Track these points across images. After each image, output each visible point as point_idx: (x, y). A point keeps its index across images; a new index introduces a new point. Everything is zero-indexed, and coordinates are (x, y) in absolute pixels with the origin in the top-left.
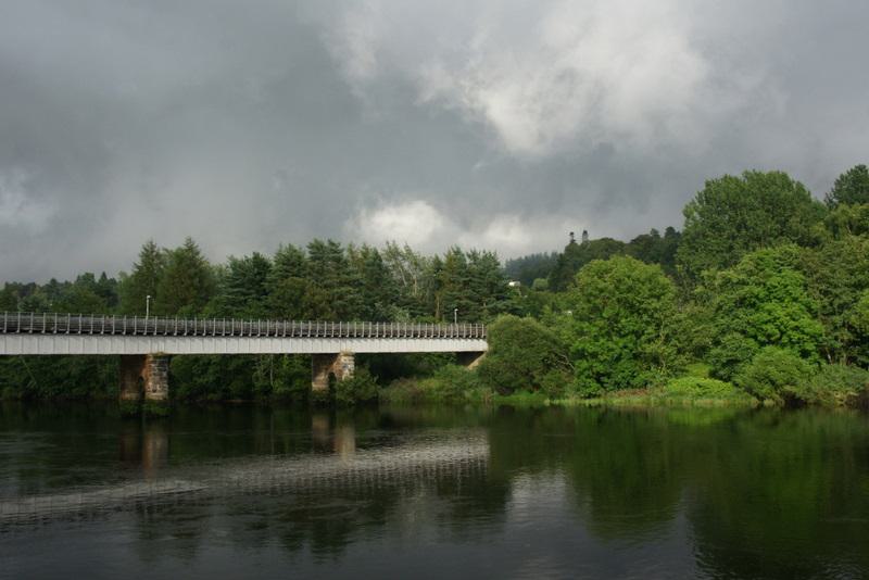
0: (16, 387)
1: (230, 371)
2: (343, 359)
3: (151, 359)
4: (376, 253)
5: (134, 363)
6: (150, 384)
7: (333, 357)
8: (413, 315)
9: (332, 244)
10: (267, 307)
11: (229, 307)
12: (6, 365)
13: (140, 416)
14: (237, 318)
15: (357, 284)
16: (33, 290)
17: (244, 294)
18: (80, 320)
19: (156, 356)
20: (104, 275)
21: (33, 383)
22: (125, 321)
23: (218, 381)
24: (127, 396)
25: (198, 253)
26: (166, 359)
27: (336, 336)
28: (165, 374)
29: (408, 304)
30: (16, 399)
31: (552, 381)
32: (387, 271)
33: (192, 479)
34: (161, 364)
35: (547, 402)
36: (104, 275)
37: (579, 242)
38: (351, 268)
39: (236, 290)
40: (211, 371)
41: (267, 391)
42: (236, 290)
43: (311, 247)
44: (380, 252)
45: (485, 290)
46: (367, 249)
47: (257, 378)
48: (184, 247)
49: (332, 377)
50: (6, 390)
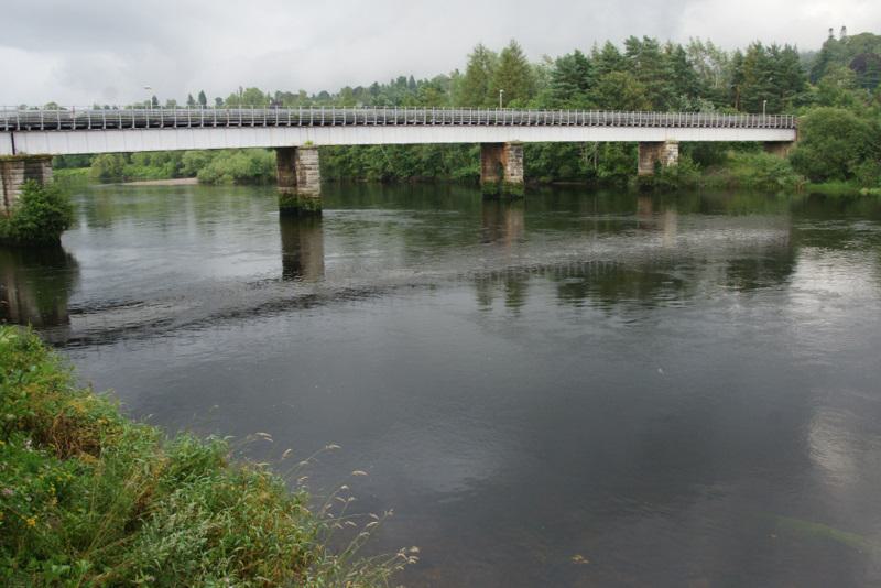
0: (377, 170)
1: (559, 158)
2: (668, 147)
3: (509, 147)
4: (680, 48)
5: (492, 150)
6: (509, 168)
7: (658, 144)
8: (717, 107)
9: (646, 39)
10: (590, 99)
11: (556, 99)
12: (369, 153)
13: (499, 199)
14: (564, 110)
15: (666, 77)
16: (361, 93)
17: (569, 88)
18: (433, 112)
19: (514, 144)
20: (412, 78)
21: (390, 168)
22: (538, 114)
23: (548, 167)
24: (489, 179)
25: (520, 53)
26: (517, 146)
27: (663, 126)
28: (521, 160)
29: (709, 96)
30: (378, 180)
31: (867, 170)
32: (690, 65)
33: (647, 250)
34: (518, 151)
35: (864, 191)
36: (412, 78)
37: (838, 37)
38: (665, 63)
39: (560, 84)
40: (543, 156)
41: (592, 175)
42: (560, 84)
43: (628, 43)
44: (684, 48)
45: (786, 83)
46: (671, 45)
47: (583, 163)
48: (509, 48)
49: (657, 165)
50: (370, 173)
